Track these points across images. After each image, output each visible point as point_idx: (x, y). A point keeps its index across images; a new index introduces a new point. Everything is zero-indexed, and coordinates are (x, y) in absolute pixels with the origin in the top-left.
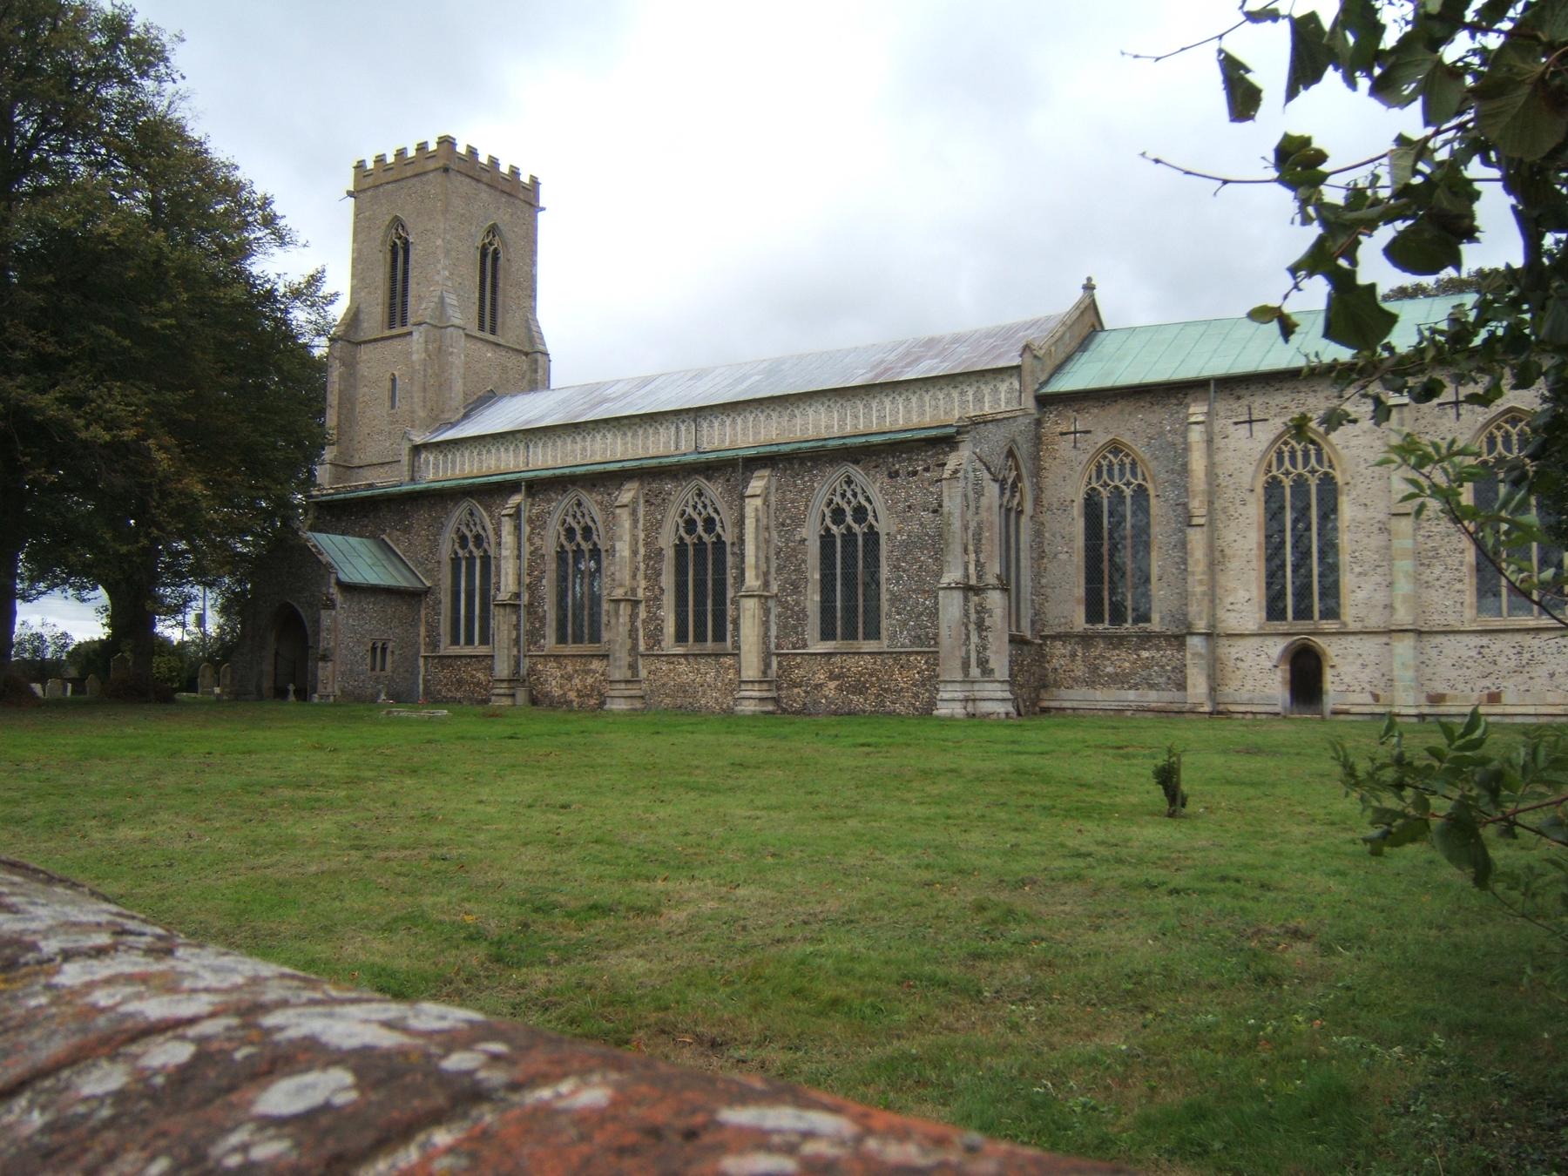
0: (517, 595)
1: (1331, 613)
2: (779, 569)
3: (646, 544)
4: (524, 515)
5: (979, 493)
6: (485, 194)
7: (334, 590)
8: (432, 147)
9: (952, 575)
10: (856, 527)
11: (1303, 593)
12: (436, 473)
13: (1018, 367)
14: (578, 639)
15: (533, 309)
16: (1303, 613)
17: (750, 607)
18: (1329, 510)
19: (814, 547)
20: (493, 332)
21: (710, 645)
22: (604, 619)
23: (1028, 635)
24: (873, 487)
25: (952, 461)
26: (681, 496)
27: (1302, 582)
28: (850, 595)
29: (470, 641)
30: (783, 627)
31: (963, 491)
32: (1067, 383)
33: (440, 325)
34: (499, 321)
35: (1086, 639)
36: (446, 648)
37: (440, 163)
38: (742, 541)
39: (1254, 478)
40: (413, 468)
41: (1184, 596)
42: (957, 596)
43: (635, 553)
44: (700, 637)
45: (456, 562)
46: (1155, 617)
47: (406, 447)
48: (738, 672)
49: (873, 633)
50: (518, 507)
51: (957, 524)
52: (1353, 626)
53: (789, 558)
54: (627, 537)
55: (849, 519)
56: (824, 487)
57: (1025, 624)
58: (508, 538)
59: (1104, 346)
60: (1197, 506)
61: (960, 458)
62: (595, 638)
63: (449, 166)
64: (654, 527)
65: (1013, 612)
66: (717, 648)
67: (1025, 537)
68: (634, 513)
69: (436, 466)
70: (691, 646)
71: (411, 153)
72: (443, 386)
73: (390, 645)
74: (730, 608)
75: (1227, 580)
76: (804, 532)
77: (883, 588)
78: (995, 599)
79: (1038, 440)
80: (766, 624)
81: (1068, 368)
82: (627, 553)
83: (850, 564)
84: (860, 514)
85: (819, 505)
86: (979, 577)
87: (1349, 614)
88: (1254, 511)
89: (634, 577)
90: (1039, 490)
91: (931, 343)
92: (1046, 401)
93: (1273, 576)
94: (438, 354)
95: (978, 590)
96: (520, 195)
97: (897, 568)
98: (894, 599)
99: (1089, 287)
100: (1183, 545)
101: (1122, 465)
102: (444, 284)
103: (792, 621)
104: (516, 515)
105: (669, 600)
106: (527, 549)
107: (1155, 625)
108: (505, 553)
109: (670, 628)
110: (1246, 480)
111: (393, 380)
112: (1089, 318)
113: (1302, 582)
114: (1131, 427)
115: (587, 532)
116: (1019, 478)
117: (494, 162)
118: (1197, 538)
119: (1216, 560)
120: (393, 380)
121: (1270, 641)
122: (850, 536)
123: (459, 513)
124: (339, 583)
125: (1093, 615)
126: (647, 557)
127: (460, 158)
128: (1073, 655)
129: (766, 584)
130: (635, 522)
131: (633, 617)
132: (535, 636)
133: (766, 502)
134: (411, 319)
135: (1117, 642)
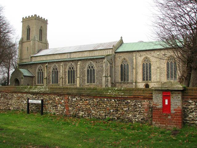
0: (47, 77)
1: (150, 80)
2: (82, 74)
3: (64, 71)
5: (107, 65)
6: (40, 22)
7: (23, 77)
8: (33, 16)
9: (104, 75)
10: (92, 69)
11: (147, 77)
12: (34, 61)
13: (112, 48)
14: (55, 83)
15: (47, 38)
16: (147, 80)
17: (78, 79)
18: (150, 68)
19: (86, 71)
20: (41, 41)
21: (73, 84)
22: (59, 80)
24: (94, 64)
26: (69, 64)
28: (91, 77)
29: (40, 83)
30: (82, 82)
31: (105, 65)
32: (118, 51)
33: (34, 40)
34: (42, 39)
35: (121, 83)
37: (35, 18)
38: (77, 70)
39: (141, 63)
40: (31, 60)
41: (133, 78)
42: (105, 78)
43: (63, 72)
45: (38, 73)
46: (129, 80)
47: (30, 57)
49: (94, 82)
50: (47, 66)
51: (105, 69)
52: (152, 81)
53: (82, 73)
54: (62, 70)
56: (88, 64)
57: (113, 81)
59: (123, 45)
60: (134, 66)
61: (105, 60)
62: (57, 83)
63: (36, 18)
64: (65, 68)
65: (111, 80)
67: (113, 70)
68: (63, 67)
69: (34, 60)
70: (70, 84)
71: (30, 16)
72: (35, 48)
73: (30, 84)
75: (138, 76)
76: (85, 69)
78: (109, 78)
79: (115, 58)
80: (80, 81)
82: (62, 72)
83: (91, 73)
84: (92, 67)
85: (68, 67)
87: (152, 80)
89: (63, 75)
91: (101, 44)
92: (115, 53)
94: (34, 44)
95: (107, 77)
96: (45, 22)
97: (97, 74)
98: (97, 78)
100: (133, 71)
101: (147, 60)
102: (34, 34)
104: (47, 67)
105: (67, 78)
106: (48, 71)
108: (45, 72)
109: (67, 82)
110: (140, 63)
111: (28, 47)
113: (147, 76)
114: (126, 56)
115: (56, 69)
117: (42, 18)
118: (134, 71)
119: (136, 74)
120: (28, 47)
121: (143, 83)
123: (39, 66)
124: (23, 75)
125: (122, 80)
126: (64, 72)
127: (37, 17)
129: (80, 76)
130: (63, 68)
131: (63, 80)
132: (49, 82)
133: (80, 66)
134: (30, 39)
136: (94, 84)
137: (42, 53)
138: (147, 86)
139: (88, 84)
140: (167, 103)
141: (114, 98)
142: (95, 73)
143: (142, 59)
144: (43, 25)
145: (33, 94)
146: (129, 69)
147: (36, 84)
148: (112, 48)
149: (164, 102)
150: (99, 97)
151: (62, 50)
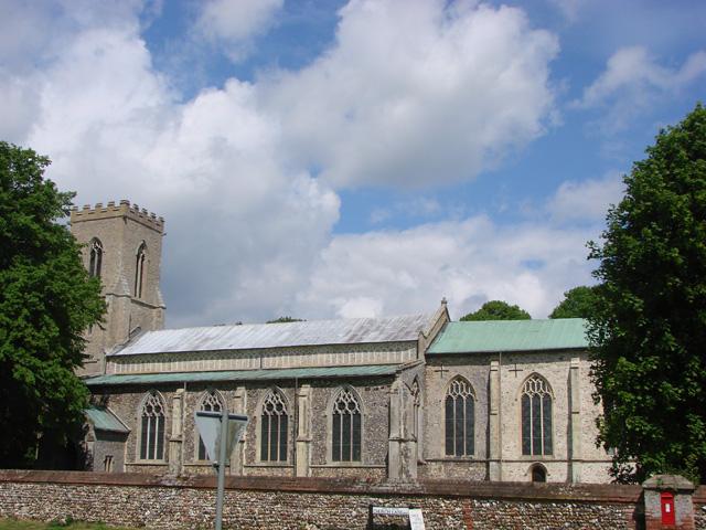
4: (185, 398)
6: (141, 228)
8: (117, 204)
11: (537, 443)
21: (464, 457)
23: (421, 460)
25: (394, 386)
27: (536, 435)
29: (151, 457)
30: (314, 455)
36: (138, 460)
44: (274, 458)
45: (145, 419)
46: (476, 453)
48: (295, 474)
49: (357, 457)
52: (557, 458)
53: (318, 423)
55: (347, 408)
58: (176, 409)
66: (283, 464)
70: (269, 462)
74: (290, 447)
77: (363, 438)
81: (437, 341)
85: (333, 401)
86: (405, 435)
88: (518, 408)
90: (426, 395)
93: (525, 433)
99: (444, 302)
103: (319, 452)
104: (181, 398)
105: (259, 440)
106: (185, 414)
107: (476, 457)
108: (174, 416)
109: (259, 454)
112: (445, 317)
113: (536, 435)
116: (418, 390)
122: (347, 415)
125: (449, 451)
128: (440, 469)
132: (190, 455)
135: (458, 462)
136: (357, 464)
137: (150, 342)
138: (539, 472)
139: (337, 464)
140: (668, 510)
141: (571, 502)
142: (363, 427)
143: (521, 381)
144: (148, 237)
145: (380, 495)
146: (476, 415)
147: (133, 459)
148: (416, 338)
149: (663, 508)
150: (496, 499)
151: (229, 338)
